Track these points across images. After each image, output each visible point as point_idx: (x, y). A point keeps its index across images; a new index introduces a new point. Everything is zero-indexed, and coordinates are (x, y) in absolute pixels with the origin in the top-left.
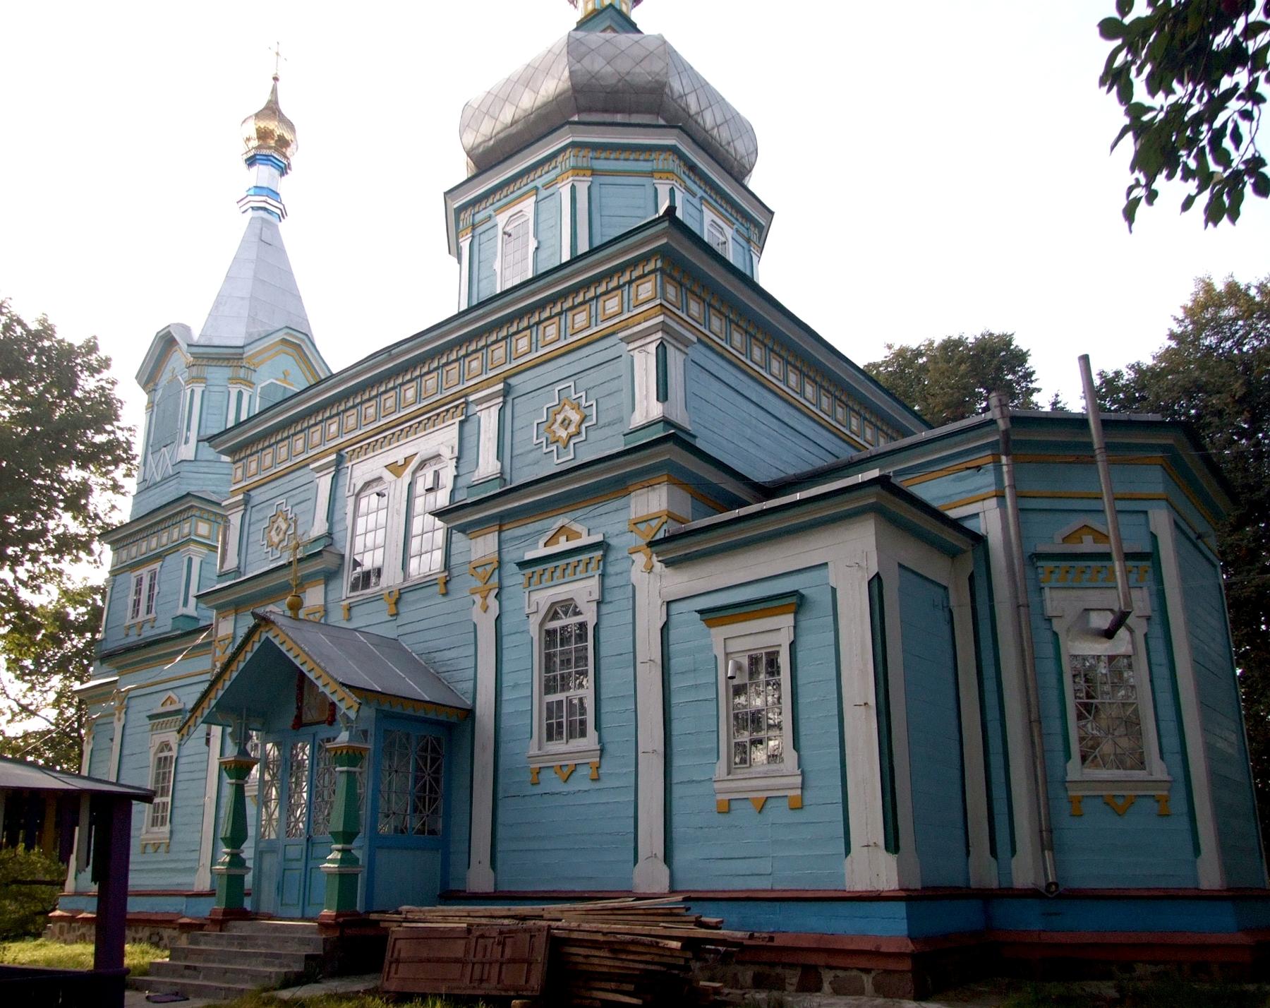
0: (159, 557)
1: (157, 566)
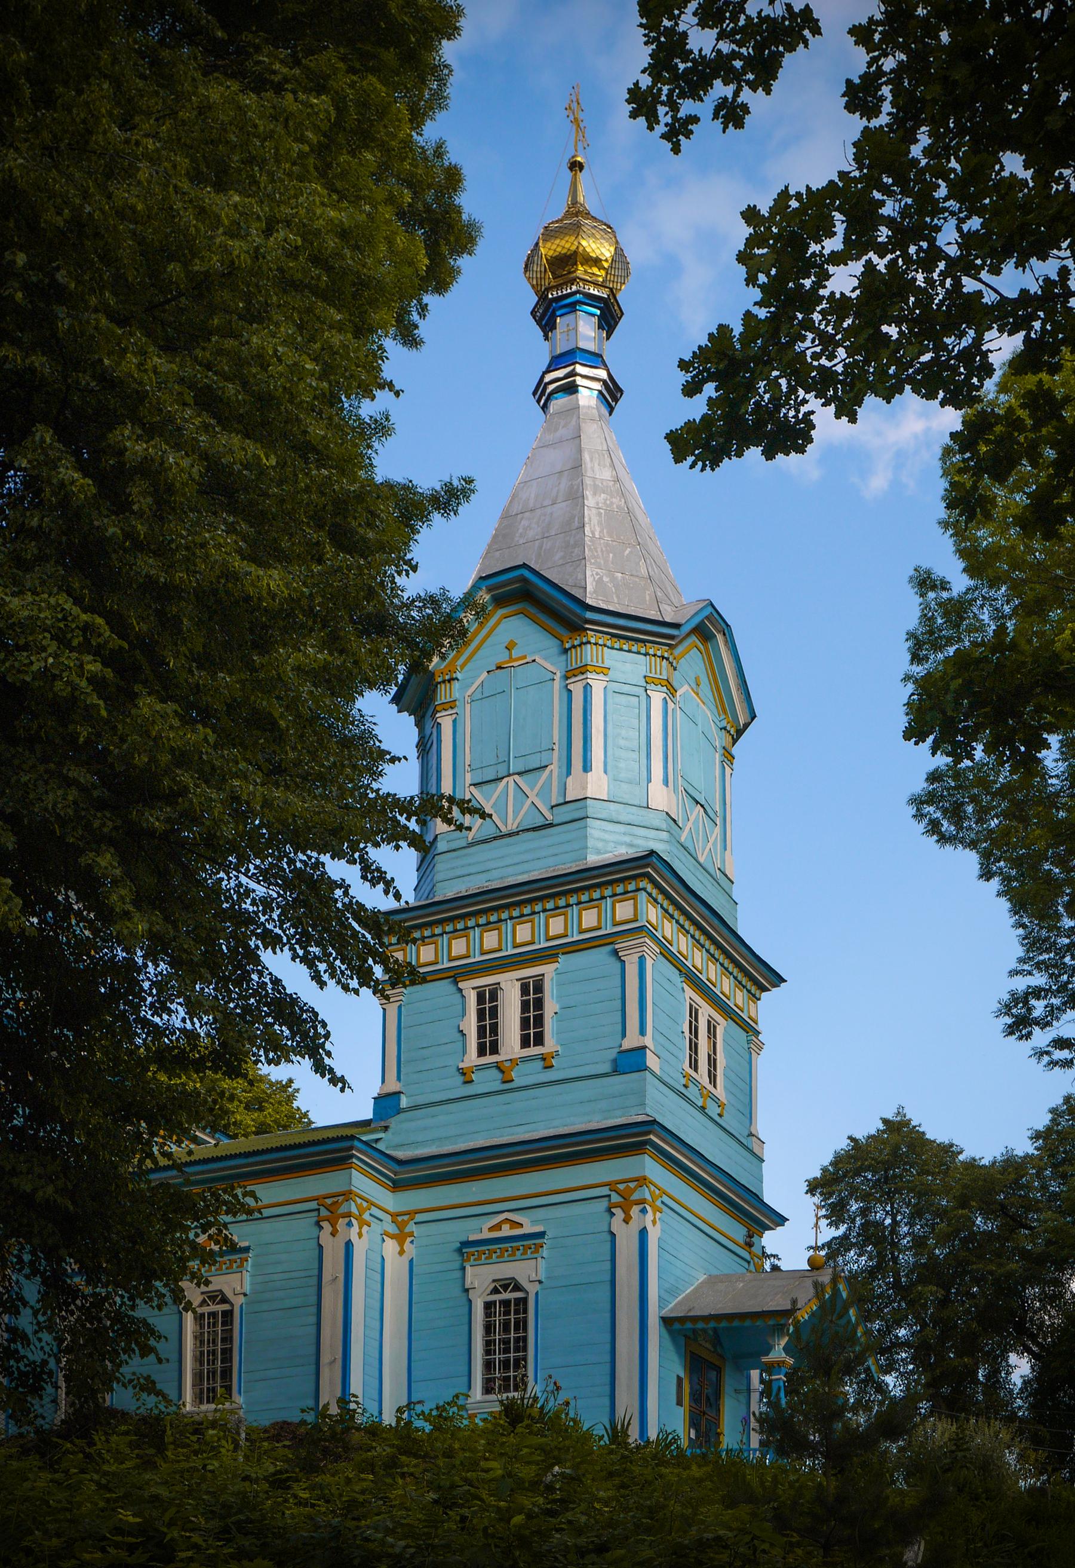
0: (547, 955)
1: (547, 970)
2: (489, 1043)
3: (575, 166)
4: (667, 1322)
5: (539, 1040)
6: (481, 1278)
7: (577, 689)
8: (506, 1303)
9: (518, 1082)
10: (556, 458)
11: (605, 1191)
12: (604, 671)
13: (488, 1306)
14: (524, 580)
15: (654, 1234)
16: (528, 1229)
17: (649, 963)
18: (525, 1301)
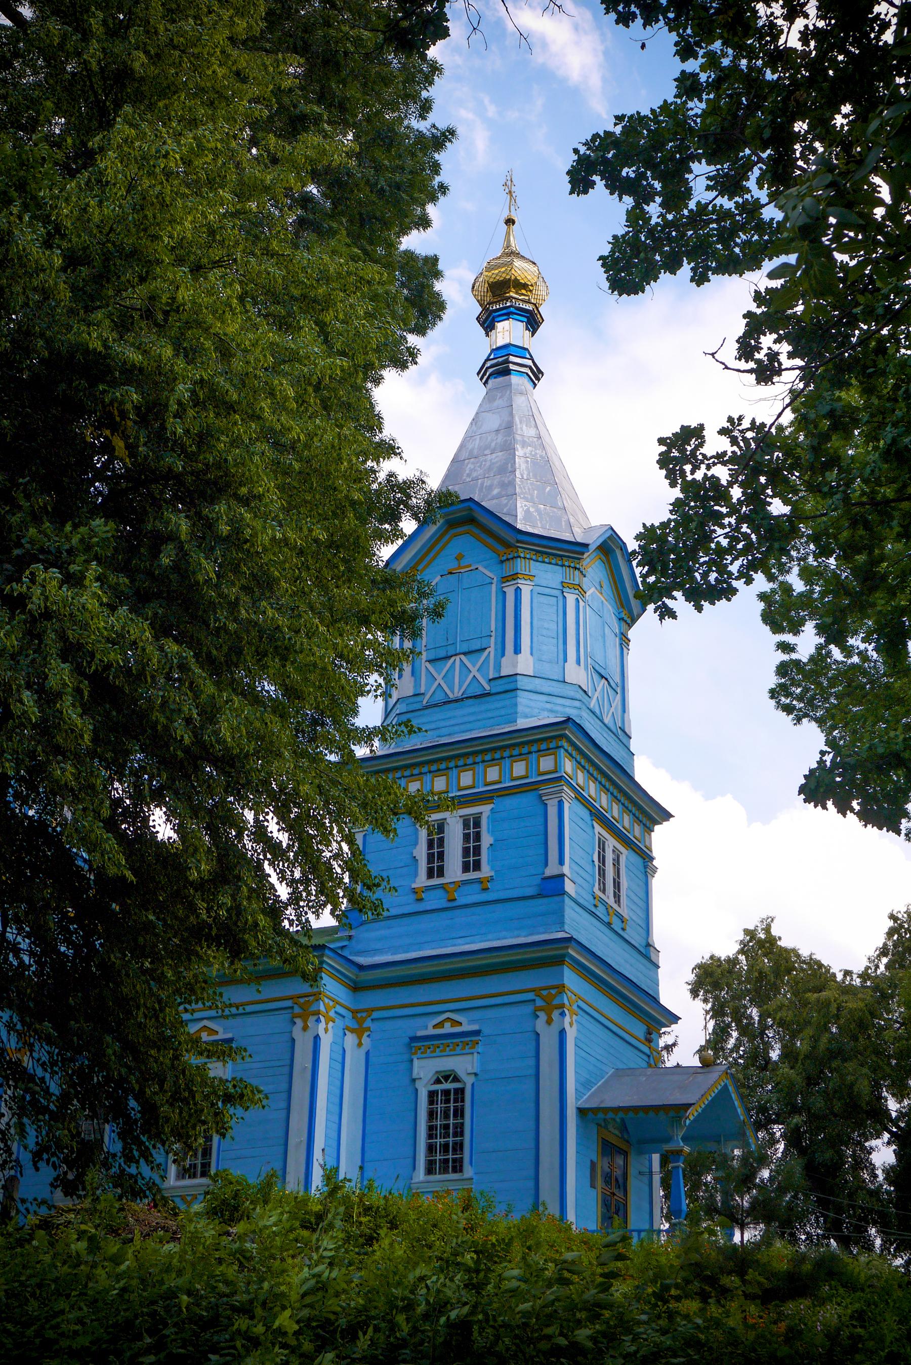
1: (485, 809)
2: (436, 869)
4: (582, 1112)
5: (477, 866)
6: (425, 1069)
8: (446, 1093)
10: (493, 422)
11: (531, 996)
12: (530, 577)
13: (432, 1095)
14: (470, 509)
15: (571, 1034)
16: (466, 1027)
17: (566, 806)
18: (460, 1092)
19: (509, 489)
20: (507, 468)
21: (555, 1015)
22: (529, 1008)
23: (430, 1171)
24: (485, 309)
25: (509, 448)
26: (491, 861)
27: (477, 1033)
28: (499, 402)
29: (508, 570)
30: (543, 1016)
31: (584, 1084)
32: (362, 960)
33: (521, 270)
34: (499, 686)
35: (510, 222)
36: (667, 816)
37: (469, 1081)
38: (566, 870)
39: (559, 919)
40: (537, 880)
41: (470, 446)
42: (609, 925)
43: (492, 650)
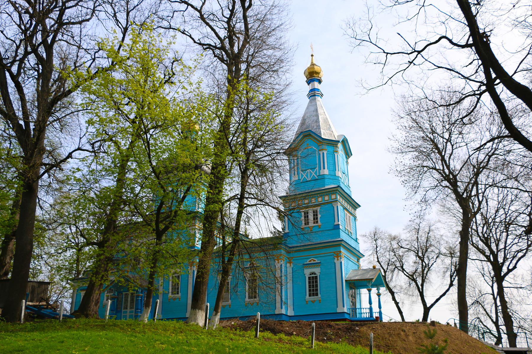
0: (319, 205)
1: (318, 209)
2: (307, 223)
3: (312, 56)
4: (346, 281)
5: (317, 222)
6: (307, 272)
7: (321, 153)
8: (313, 277)
9: (314, 231)
10: (312, 109)
11: (333, 254)
12: (326, 150)
13: (309, 278)
15: (343, 262)
16: (317, 261)
18: (317, 277)
19: (319, 127)
20: (317, 121)
21: (339, 258)
22: (333, 257)
23: (310, 296)
24: (307, 79)
25: (317, 116)
26: (320, 221)
27: (320, 263)
28: (313, 103)
29: (321, 147)
30: (336, 259)
31: (346, 274)
32: (290, 246)
33: (316, 69)
34: (320, 177)
35: (312, 56)
36: (360, 206)
37: (318, 274)
38: (340, 223)
39: (339, 236)
40: (333, 226)
41: (307, 115)
42: (348, 235)
43: (317, 168)
